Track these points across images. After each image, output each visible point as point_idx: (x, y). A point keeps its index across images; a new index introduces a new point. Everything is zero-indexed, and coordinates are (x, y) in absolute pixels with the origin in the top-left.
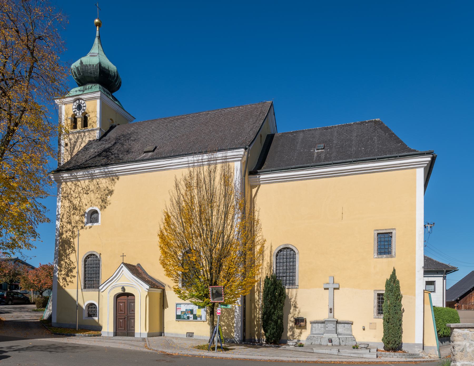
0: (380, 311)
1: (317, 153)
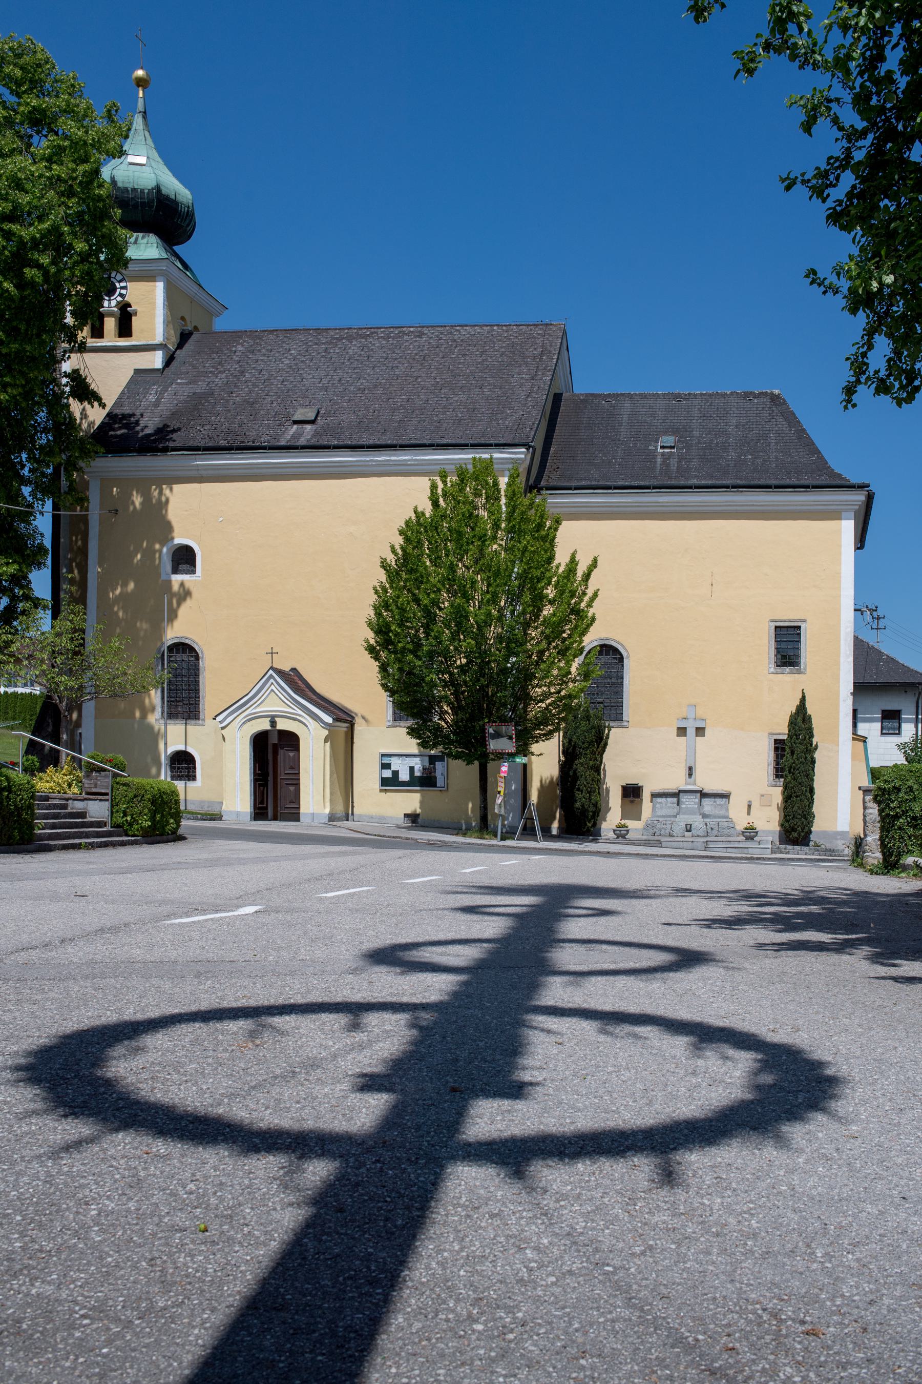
0: (779, 771)
1: (663, 454)
